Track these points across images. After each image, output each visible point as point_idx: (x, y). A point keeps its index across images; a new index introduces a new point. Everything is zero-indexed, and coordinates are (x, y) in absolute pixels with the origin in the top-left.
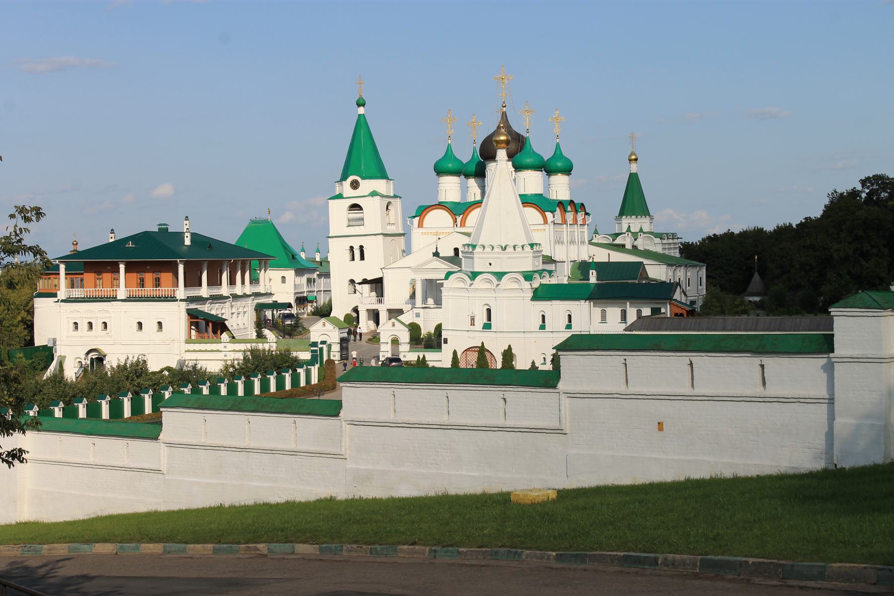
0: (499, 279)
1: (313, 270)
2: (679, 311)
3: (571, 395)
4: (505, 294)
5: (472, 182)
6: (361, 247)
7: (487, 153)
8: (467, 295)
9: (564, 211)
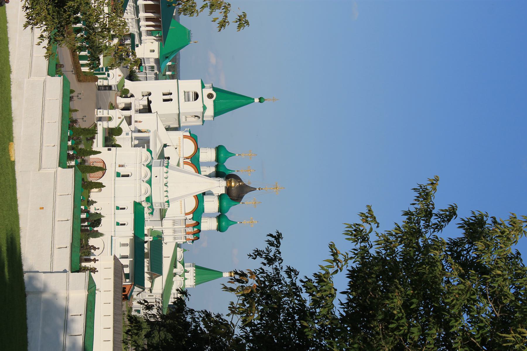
1: (159, 69)
2: (127, 290)
3: (56, 173)
4: (138, 185)
5: (213, 170)
6: (171, 100)
7: (228, 177)
8: (138, 162)
9: (194, 226)
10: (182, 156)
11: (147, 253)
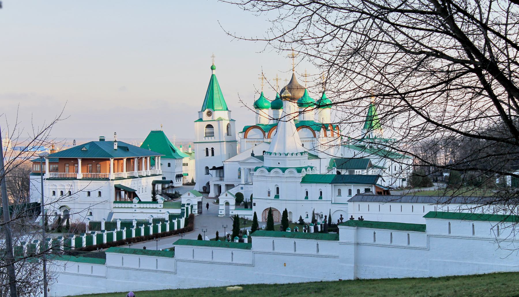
0: (284, 172)
2: (380, 191)
6: (212, 149)
11: (350, 172)
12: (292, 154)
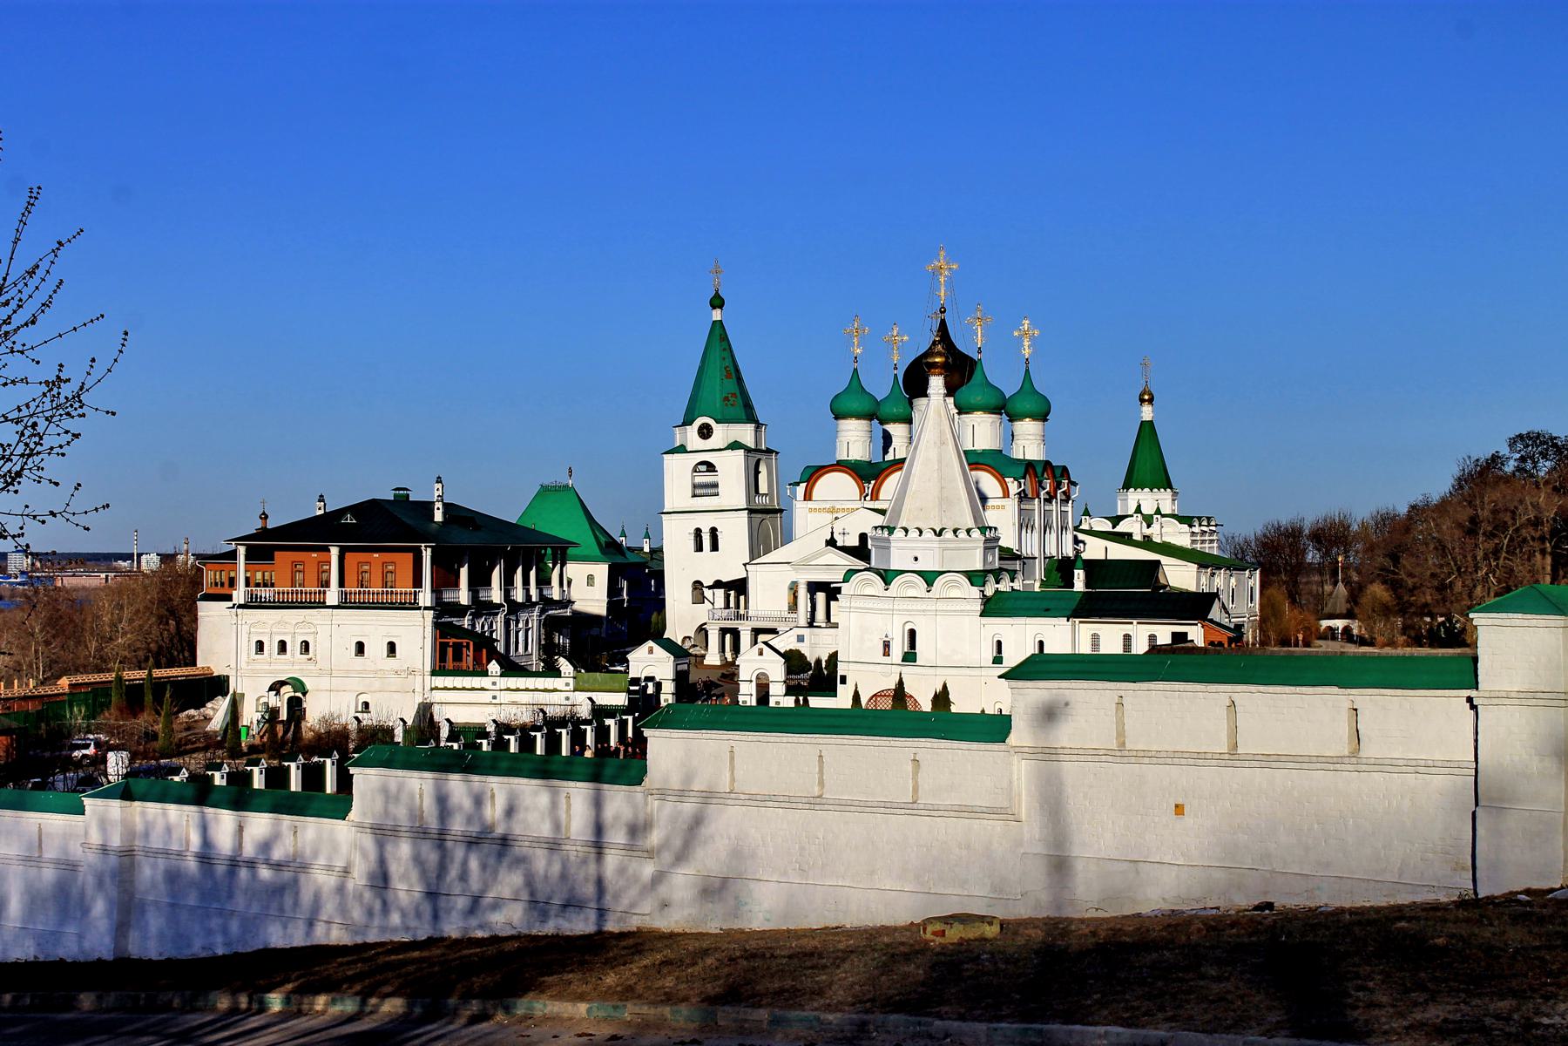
6: (714, 531)
7: (915, 383)
10: (858, 504)
12: (955, 531)
